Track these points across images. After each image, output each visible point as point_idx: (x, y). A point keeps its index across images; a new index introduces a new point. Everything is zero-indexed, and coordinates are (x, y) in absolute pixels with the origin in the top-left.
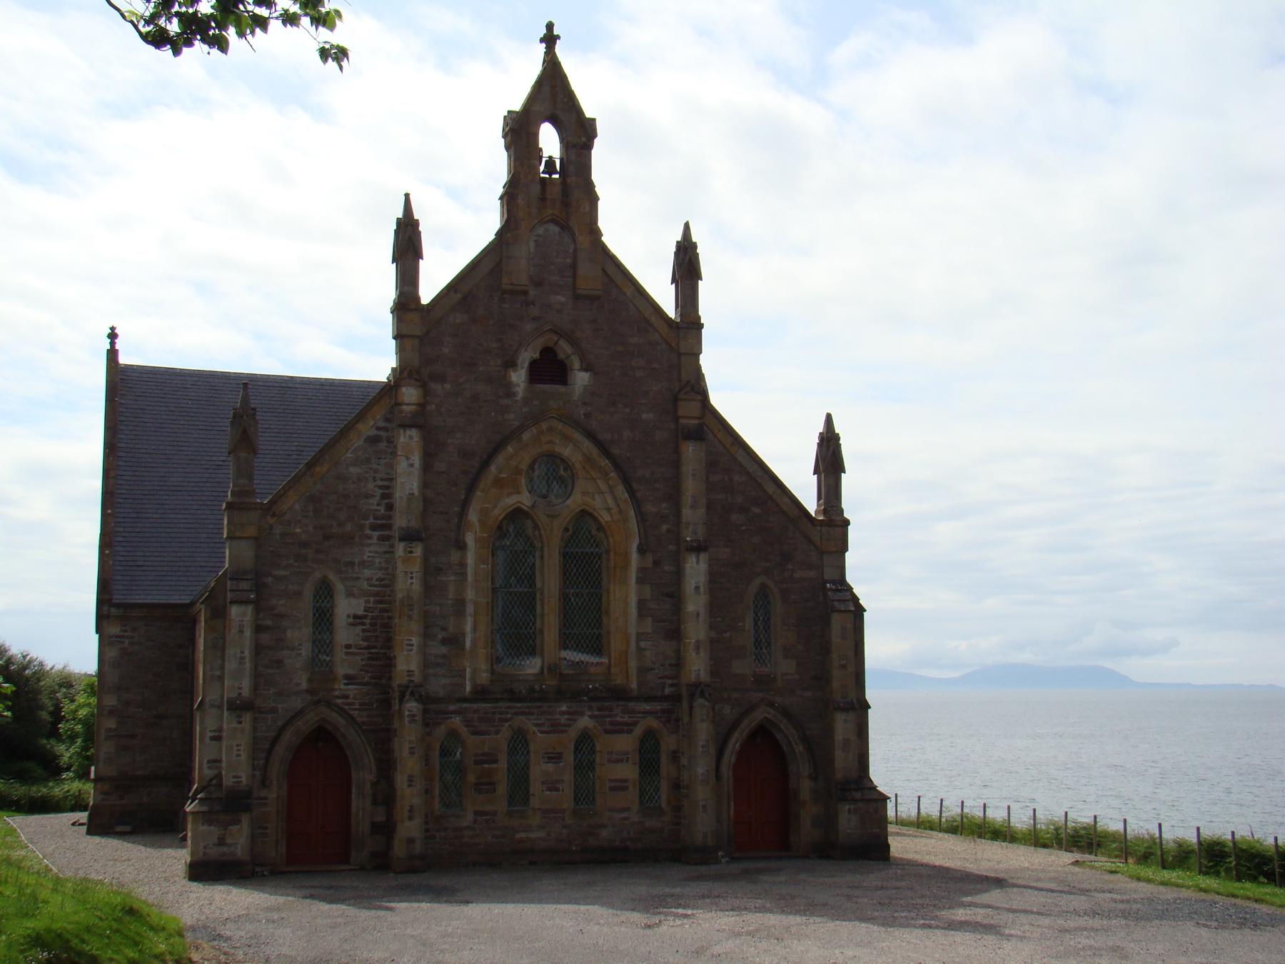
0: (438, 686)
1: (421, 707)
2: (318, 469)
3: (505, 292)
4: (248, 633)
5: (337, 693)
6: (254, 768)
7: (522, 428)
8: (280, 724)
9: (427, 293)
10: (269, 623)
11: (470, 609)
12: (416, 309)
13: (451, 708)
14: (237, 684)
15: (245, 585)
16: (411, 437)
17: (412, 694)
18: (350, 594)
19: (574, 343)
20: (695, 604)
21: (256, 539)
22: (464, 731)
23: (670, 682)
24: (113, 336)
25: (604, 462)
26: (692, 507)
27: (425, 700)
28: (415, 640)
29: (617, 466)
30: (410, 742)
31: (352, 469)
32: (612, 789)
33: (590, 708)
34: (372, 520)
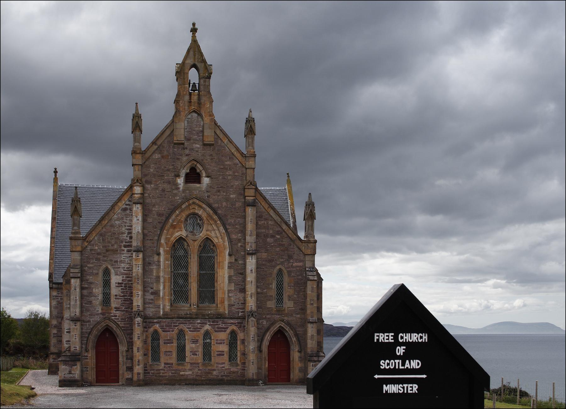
10: (86, 286)
11: (162, 280)
18: (116, 274)
22: (160, 330)
26: (250, 235)
29: (220, 218)
33: (209, 321)
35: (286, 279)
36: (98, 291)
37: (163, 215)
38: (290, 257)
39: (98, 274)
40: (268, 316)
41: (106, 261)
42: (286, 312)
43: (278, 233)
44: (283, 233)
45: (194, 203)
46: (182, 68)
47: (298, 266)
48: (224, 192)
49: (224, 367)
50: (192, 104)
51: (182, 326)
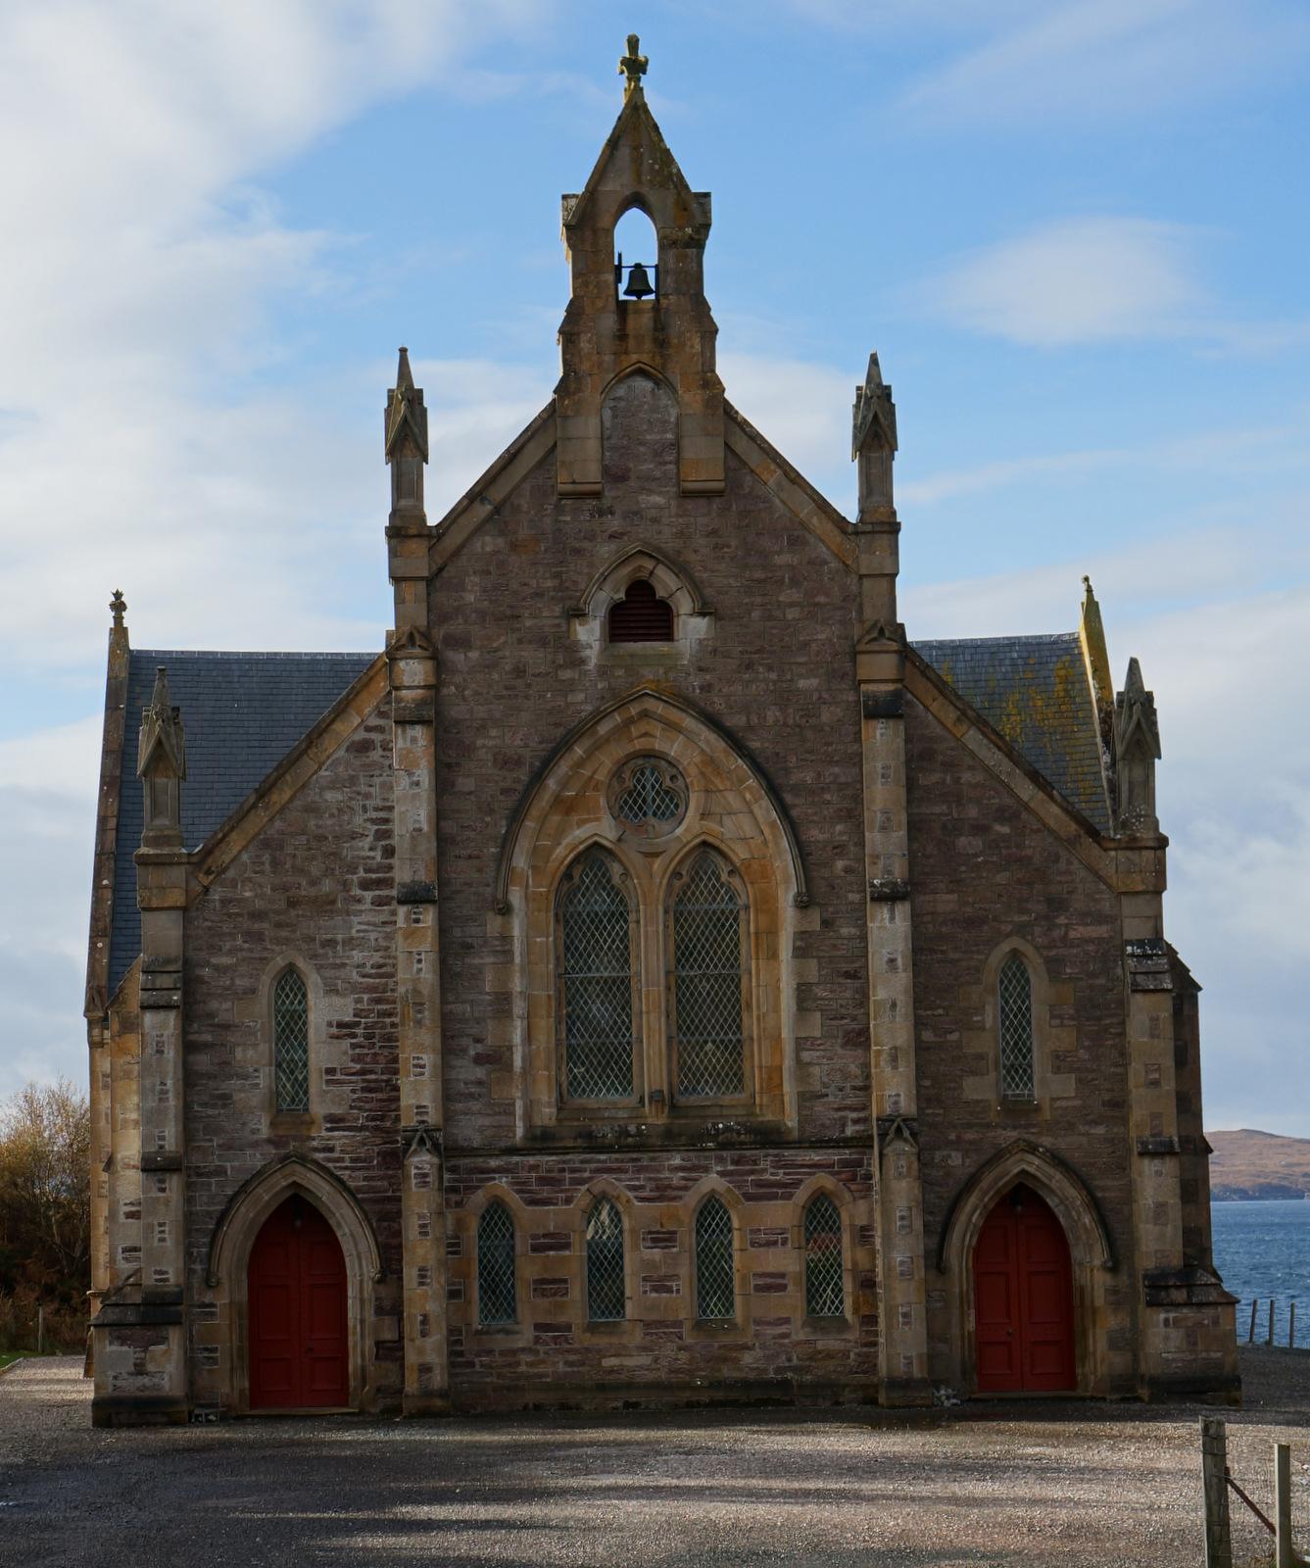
0: (471, 1129)
1: (436, 1160)
2: (275, 797)
3: (564, 495)
4: (171, 1053)
5: (315, 1143)
6: (188, 1255)
7: (599, 716)
8: (230, 1192)
9: (435, 513)
10: (208, 1038)
11: (519, 1007)
12: (419, 536)
13: (493, 1163)
14: (156, 1132)
15: (165, 981)
16: (414, 740)
17: (422, 1142)
18: (332, 990)
19: (680, 569)
20: (890, 986)
21: (185, 909)
22: (514, 1200)
23: (854, 1115)
24: (118, 606)
26: (884, 829)
27: (449, 1152)
28: (427, 1059)
29: (758, 769)
30: (421, 1217)
31: (329, 796)
32: (758, 1288)
33: (721, 1160)
34: (362, 873)
40: (970, 1136)
41: (287, 941)
42: (1047, 1115)
44: (1024, 815)
45: (645, 714)
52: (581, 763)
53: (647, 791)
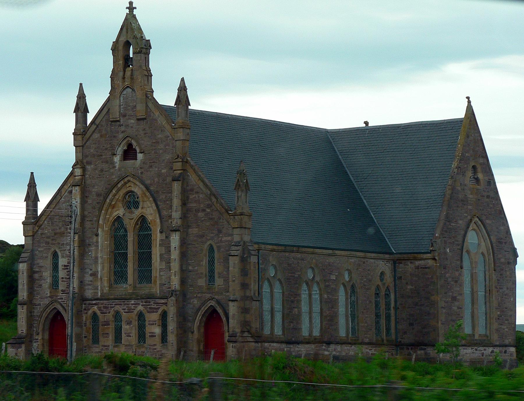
10: (37, 270)
11: (100, 261)
18: (63, 257)
22: (98, 312)
25: (148, 194)
26: (176, 211)
29: (152, 196)
33: (142, 302)
35: (216, 255)
36: (47, 274)
37: (101, 195)
38: (220, 231)
39: (47, 257)
40: (199, 295)
41: (54, 244)
42: (216, 290)
43: (209, 206)
44: (213, 206)
45: (129, 181)
46: (116, 46)
47: (227, 241)
48: (156, 167)
49: (156, 349)
50: (126, 79)
51: (117, 308)
52: (115, 195)
53: (131, 202)
